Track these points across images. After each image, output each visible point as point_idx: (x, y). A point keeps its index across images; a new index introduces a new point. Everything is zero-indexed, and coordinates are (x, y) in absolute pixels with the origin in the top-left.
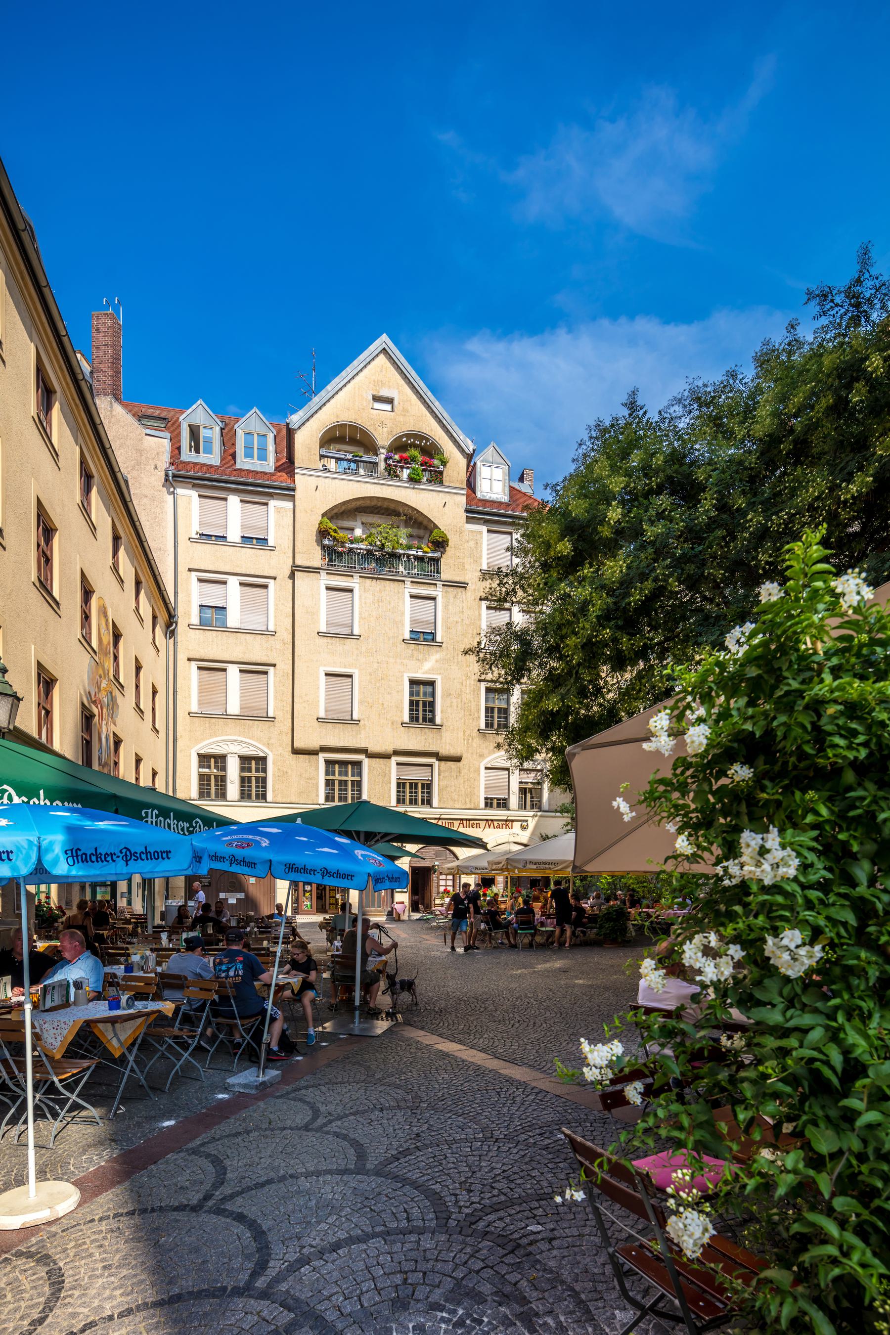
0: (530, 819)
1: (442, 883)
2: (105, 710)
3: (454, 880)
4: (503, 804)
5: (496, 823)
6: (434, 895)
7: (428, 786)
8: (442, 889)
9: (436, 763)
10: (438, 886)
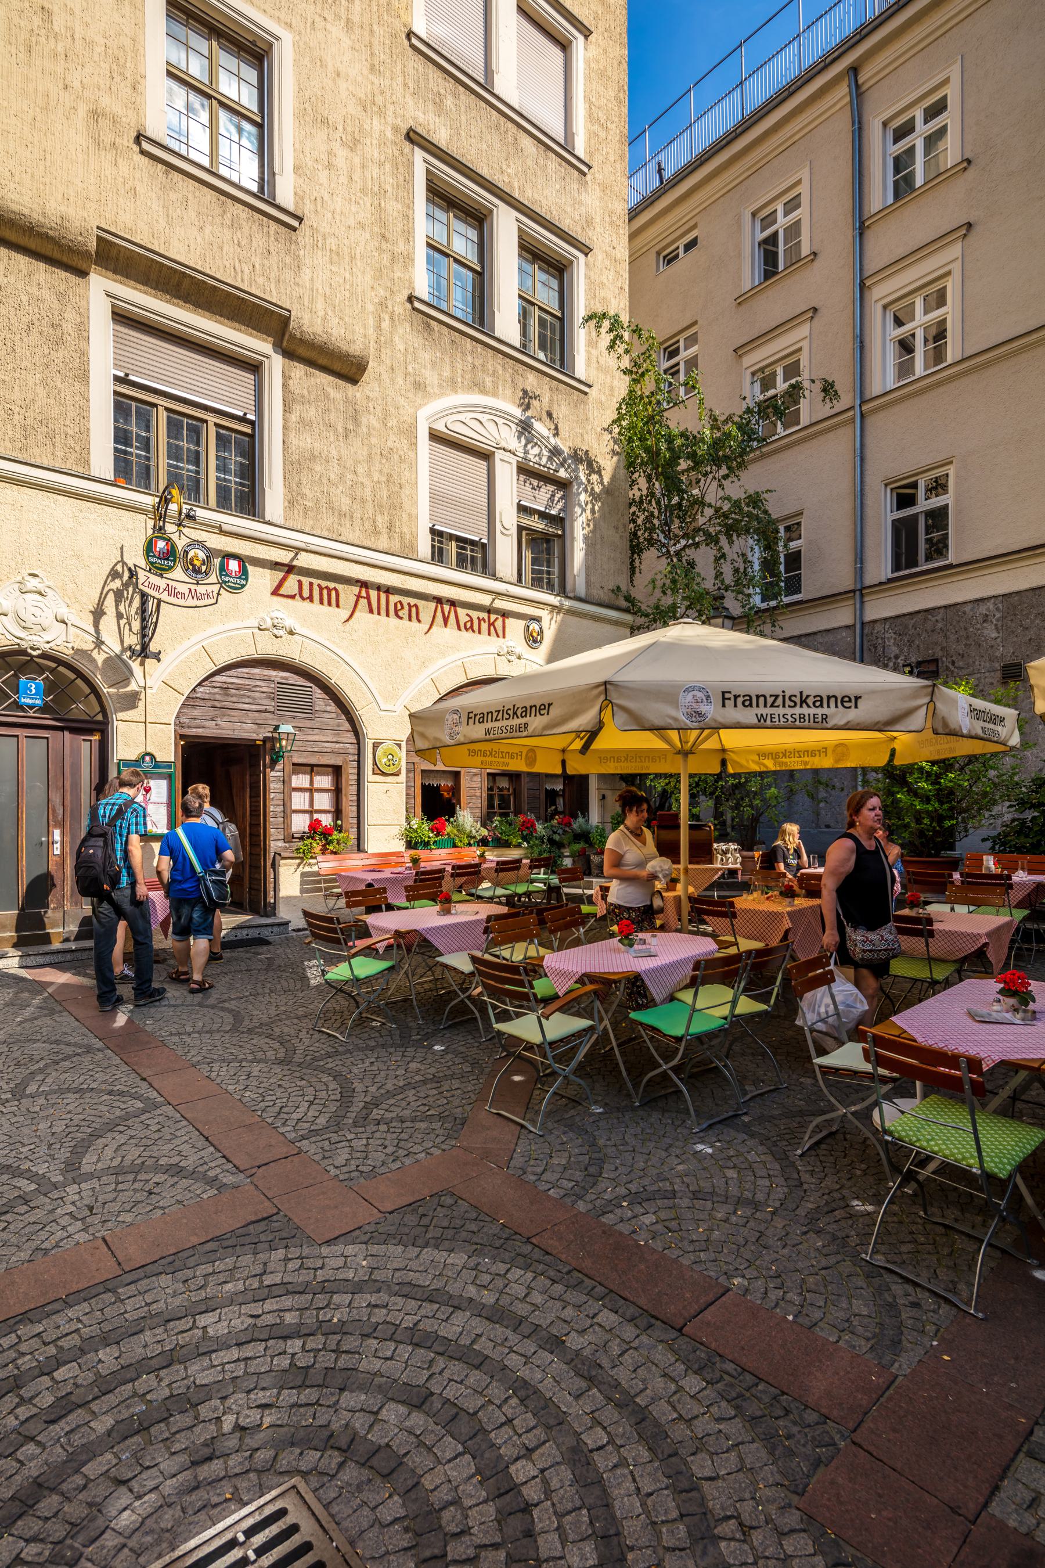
0: (544, 614)
1: (299, 801)
2: (234, 1353)
3: (337, 792)
4: (475, 555)
5: (462, 612)
6: (275, 845)
7: (245, 444)
8: (300, 823)
9: (276, 365)
10: (287, 812)
